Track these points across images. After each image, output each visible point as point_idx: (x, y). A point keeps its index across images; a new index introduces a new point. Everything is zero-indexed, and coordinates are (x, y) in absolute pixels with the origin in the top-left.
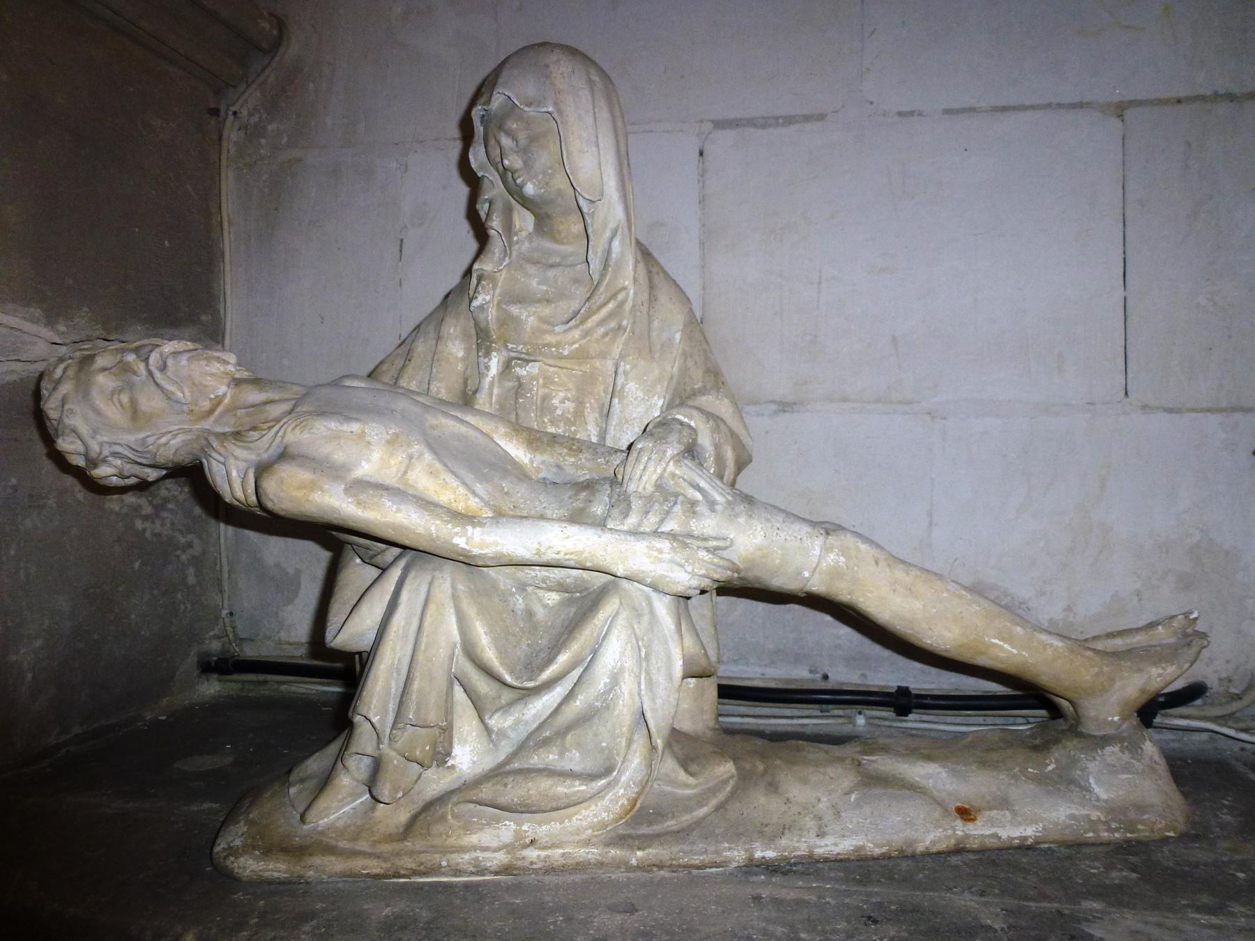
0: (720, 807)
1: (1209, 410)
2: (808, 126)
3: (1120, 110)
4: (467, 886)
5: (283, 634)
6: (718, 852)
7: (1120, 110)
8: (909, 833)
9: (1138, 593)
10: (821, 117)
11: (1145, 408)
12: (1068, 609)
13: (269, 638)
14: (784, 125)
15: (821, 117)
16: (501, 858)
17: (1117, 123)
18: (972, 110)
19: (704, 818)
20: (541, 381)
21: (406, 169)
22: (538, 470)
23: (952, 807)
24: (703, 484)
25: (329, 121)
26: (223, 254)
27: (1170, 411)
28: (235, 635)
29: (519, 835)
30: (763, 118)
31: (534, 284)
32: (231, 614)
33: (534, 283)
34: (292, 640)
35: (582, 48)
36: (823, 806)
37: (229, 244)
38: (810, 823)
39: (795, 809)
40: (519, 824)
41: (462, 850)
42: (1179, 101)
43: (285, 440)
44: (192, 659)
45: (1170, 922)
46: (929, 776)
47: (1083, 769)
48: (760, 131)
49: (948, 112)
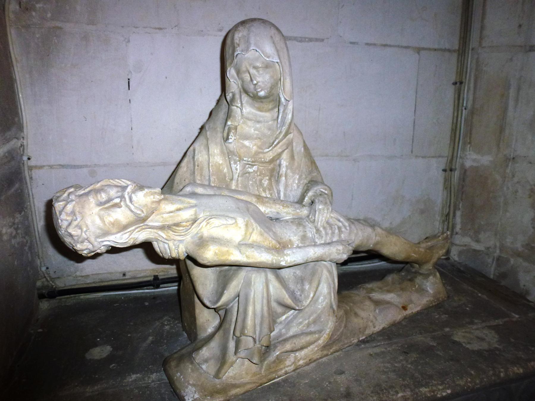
0: (345, 326)
1: (433, 157)
2: (317, 43)
3: (419, 50)
4: (283, 380)
5: (78, 274)
6: (351, 342)
7: (419, 50)
8: (395, 319)
9: (410, 216)
10: (322, 40)
11: (417, 156)
12: (391, 223)
13: (70, 276)
14: (308, 42)
15: (322, 40)
16: (292, 368)
17: (417, 55)
18: (375, 45)
19: (343, 331)
20: (258, 173)
21: (129, 41)
22: (268, 213)
23: (400, 306)
24: (342, 220)
25: (78, 8)
26: (16, 80)
27: (423, 157)
28: (50, 277)
29: (296, 357)
30: (300, 37)
31: (253, 131)
32: (47, 268)
33: (252, 130)
34: (83, 275)
35: (281, 29)
36: (371, 317)
37: (19, 73)
38: (371, 324)
39: (365, 320)
40: (295, 354)
41: (281, 369)
42: (435, 50)
43: (202, 230)
44: (36, 295)
45: (468, 330)
46: (392, 298)
47: (425, 285)
48: (300, 44)
49: (367, 44)
